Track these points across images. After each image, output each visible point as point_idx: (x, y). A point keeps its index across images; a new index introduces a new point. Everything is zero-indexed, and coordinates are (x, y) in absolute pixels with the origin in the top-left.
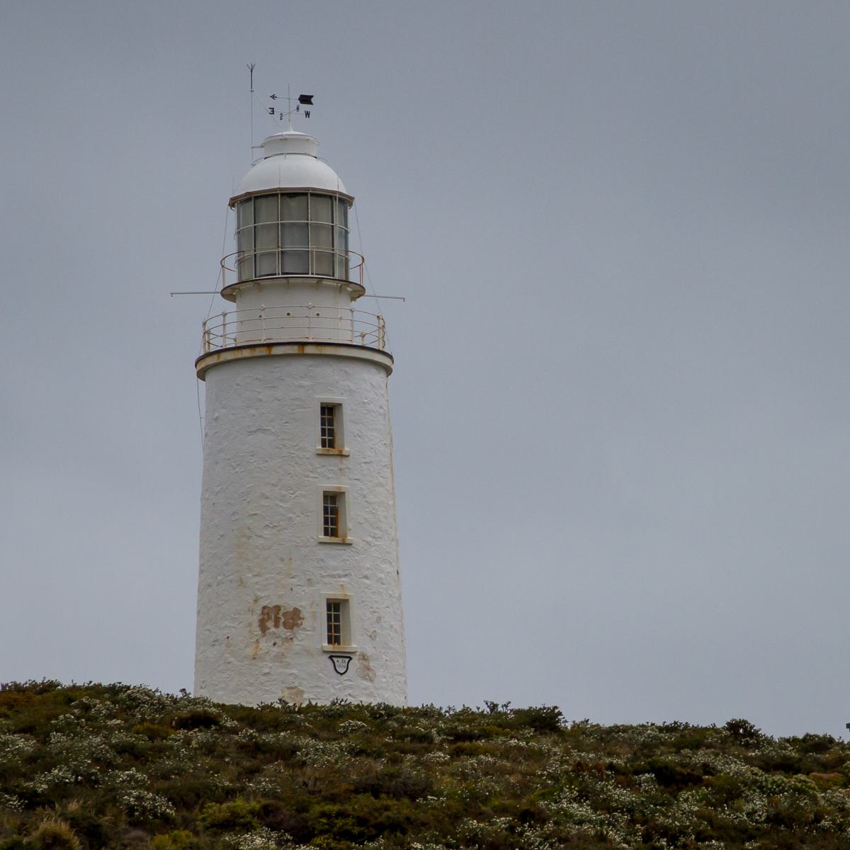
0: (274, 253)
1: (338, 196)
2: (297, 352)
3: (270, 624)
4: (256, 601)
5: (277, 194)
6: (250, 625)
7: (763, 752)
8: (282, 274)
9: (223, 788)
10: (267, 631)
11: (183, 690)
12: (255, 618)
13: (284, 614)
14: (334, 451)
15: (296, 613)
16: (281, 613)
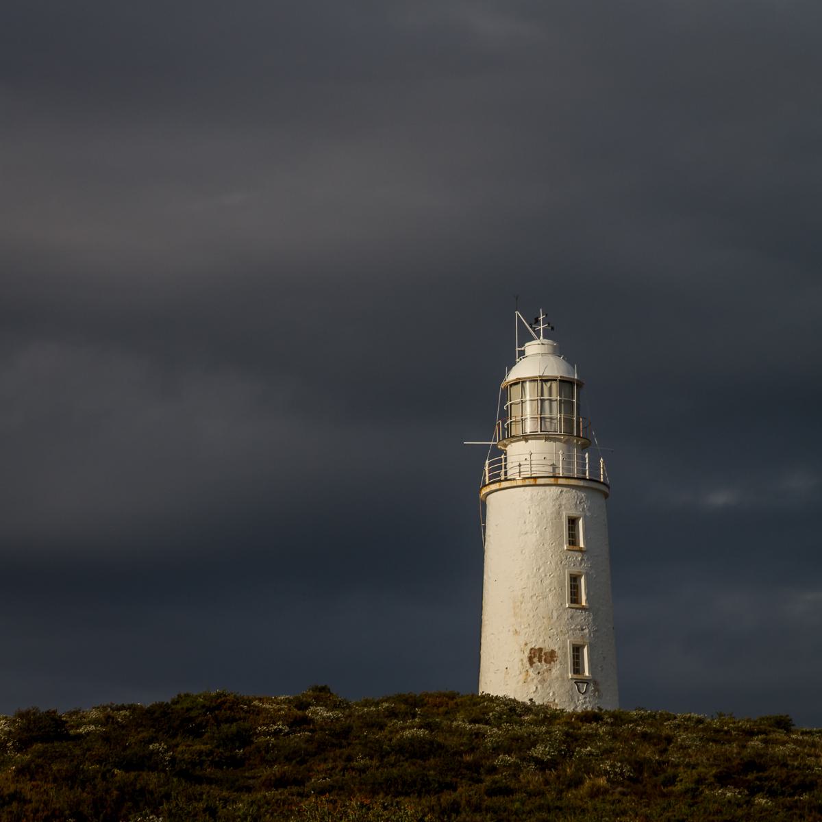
0: (537, 418)
1: (538, 378)
2: (553, 483)
3: (536, 660)
4: (526, 644)
5: (537, 380)
6: (522, 660)
7: (502, 775)
8: (541, 431)
9: (656, 760)
10: (534, 665)
11: (531, 700)
12: (527, 654)
13: (545, 654)
14: (575, 548)
15: (553, 652)
16: (543, 653)
